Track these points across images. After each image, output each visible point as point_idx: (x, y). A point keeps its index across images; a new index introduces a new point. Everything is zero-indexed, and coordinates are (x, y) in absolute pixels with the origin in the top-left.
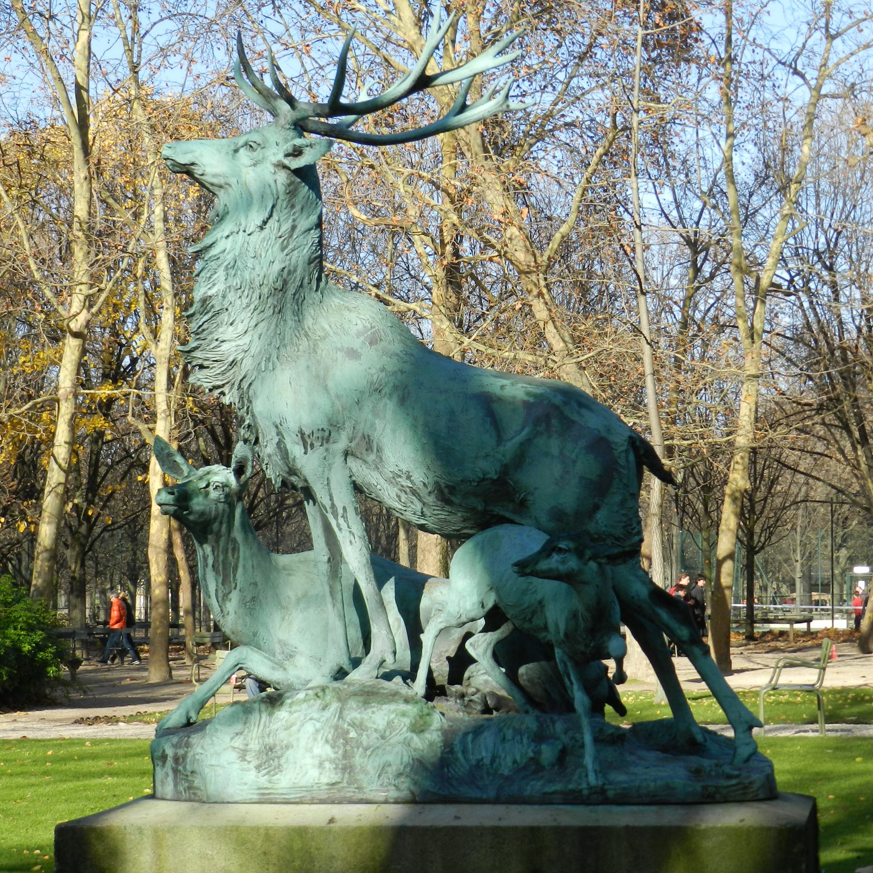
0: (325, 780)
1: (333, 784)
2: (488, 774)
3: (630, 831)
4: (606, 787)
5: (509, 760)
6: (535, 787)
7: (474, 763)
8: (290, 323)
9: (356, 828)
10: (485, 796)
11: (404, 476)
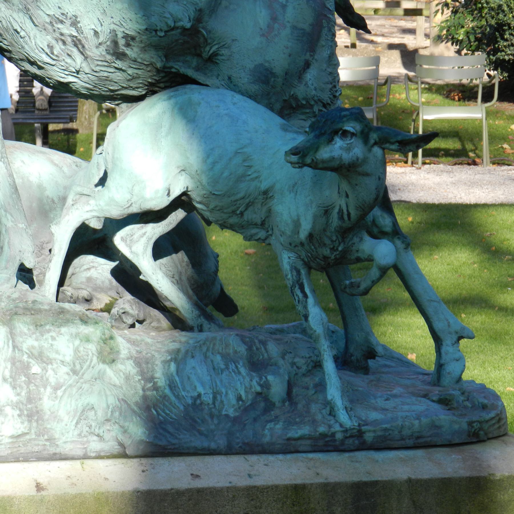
1: (19, 436)
2: (212, 416)
3: (414, 485)
4: (364, 428)
6: (273, 431)
7: (190, 401)
9: (75, 496)
10: (213, 446)
11: (68, 22)
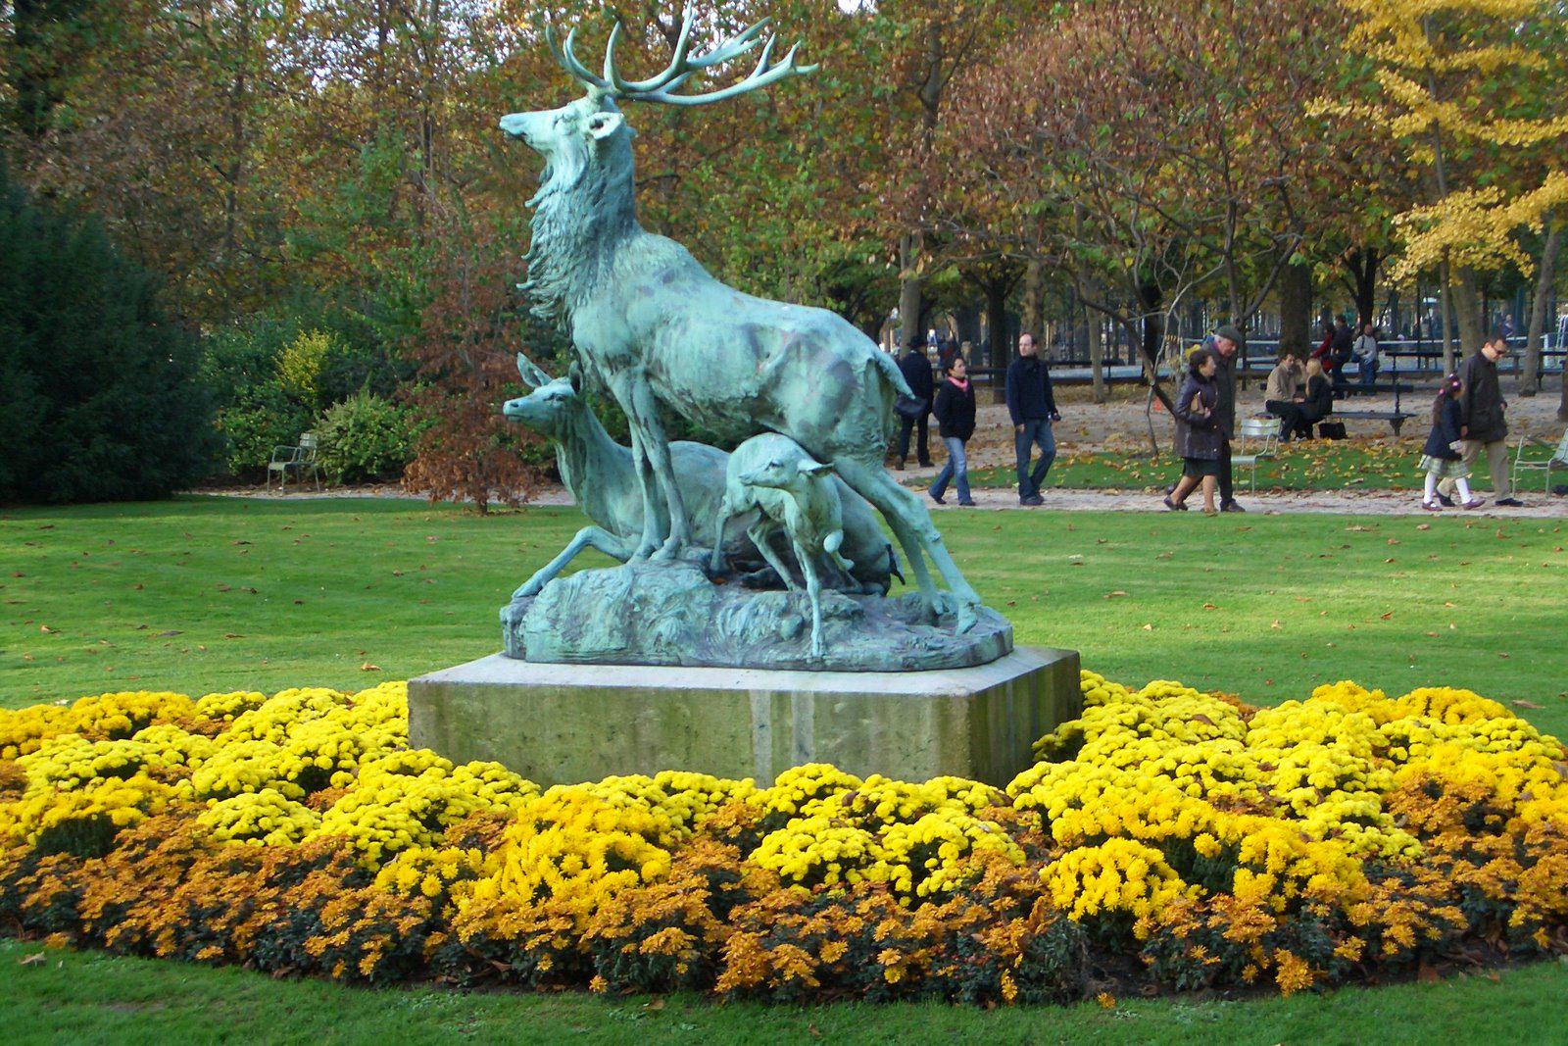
0: (613, 646)
5: (756, 633)
8: (601, 265)
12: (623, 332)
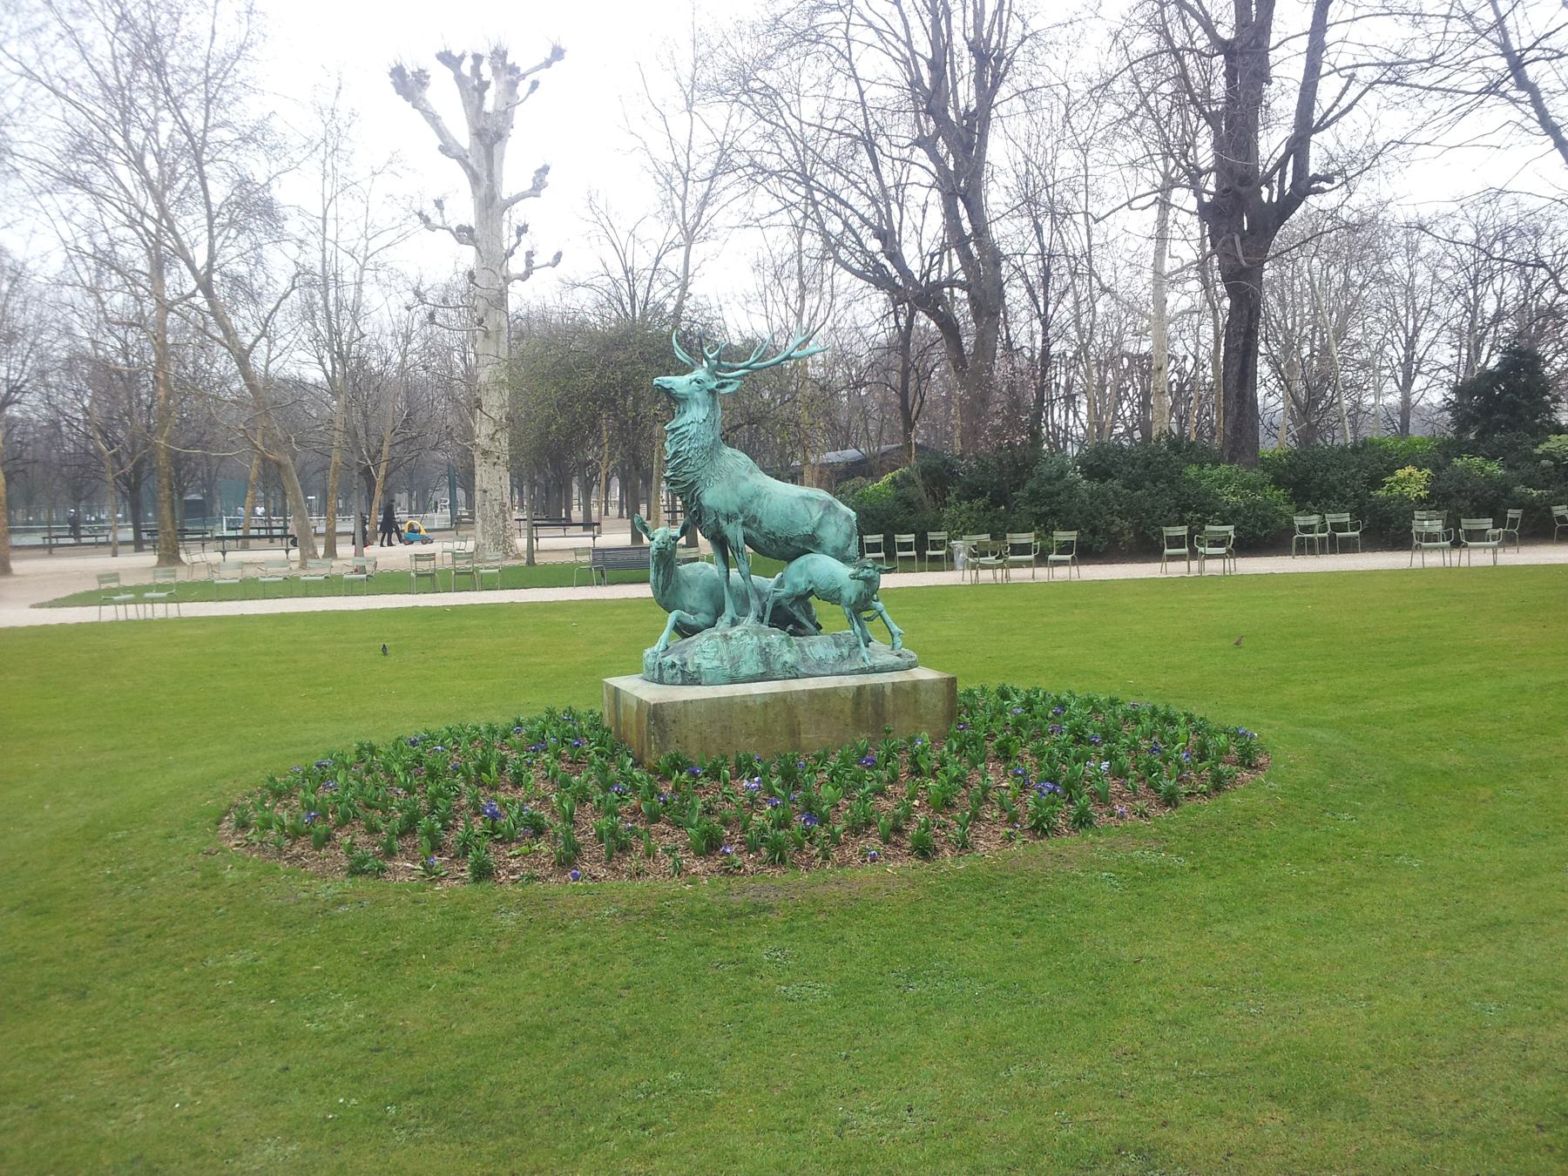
12: (738, 500)
